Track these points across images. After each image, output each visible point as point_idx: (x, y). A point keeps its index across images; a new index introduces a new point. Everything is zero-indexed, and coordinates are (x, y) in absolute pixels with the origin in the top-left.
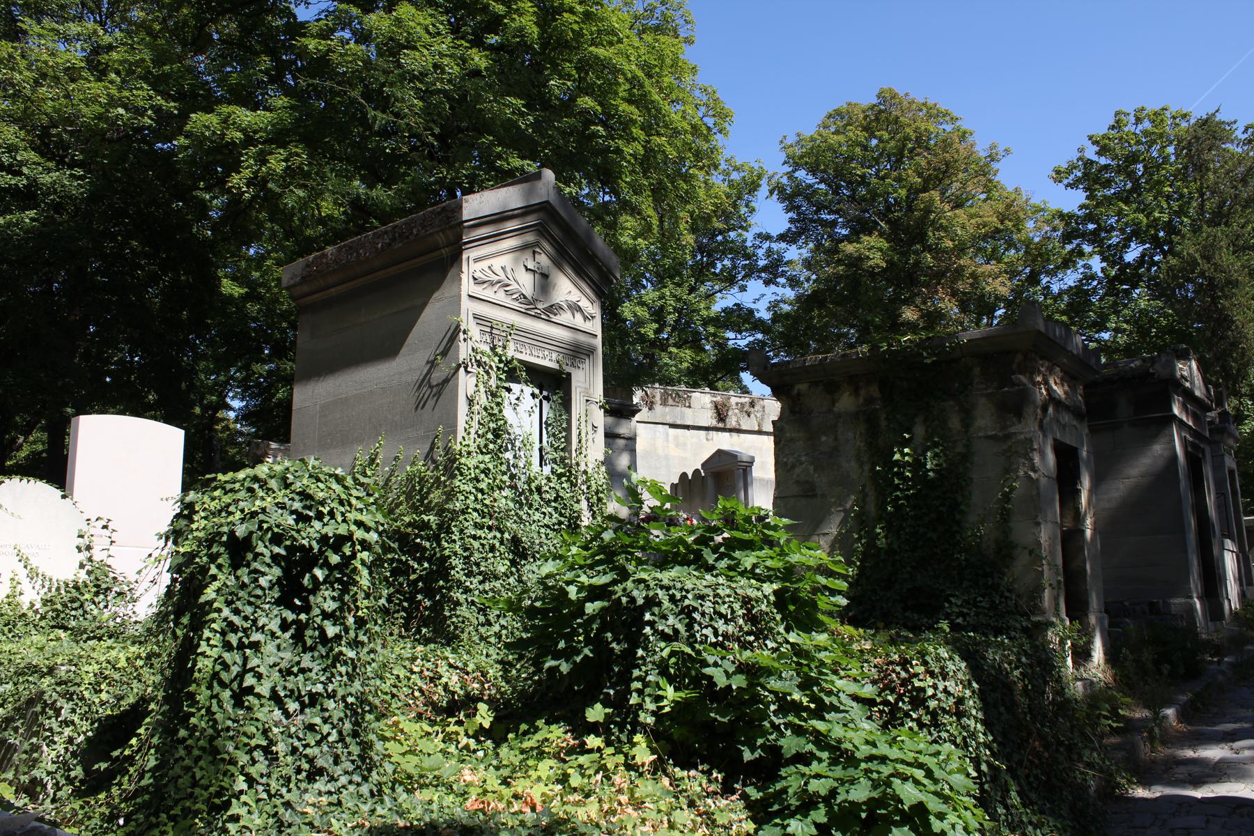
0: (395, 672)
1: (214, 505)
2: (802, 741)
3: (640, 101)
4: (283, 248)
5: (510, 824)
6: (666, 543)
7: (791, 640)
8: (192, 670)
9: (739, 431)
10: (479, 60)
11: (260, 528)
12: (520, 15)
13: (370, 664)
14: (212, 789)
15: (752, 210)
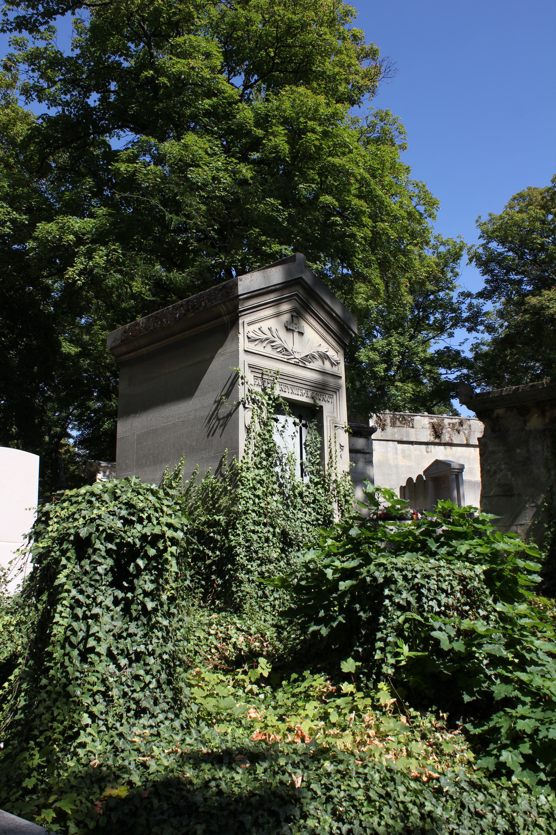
0: (197, 634)
1: (64, 513)
2: (510, 688)
3: (367, 195)
4: (106, 318)
5: (286, 751)
6: (399, 535)
7: (498, 609)
8: (50, 635)
9: (451, 445)
10: (246, 172)
11: (97, 530)
12: (275, 136)
13: (179, 630)
14: (66, 723)
15: (456, 275)
